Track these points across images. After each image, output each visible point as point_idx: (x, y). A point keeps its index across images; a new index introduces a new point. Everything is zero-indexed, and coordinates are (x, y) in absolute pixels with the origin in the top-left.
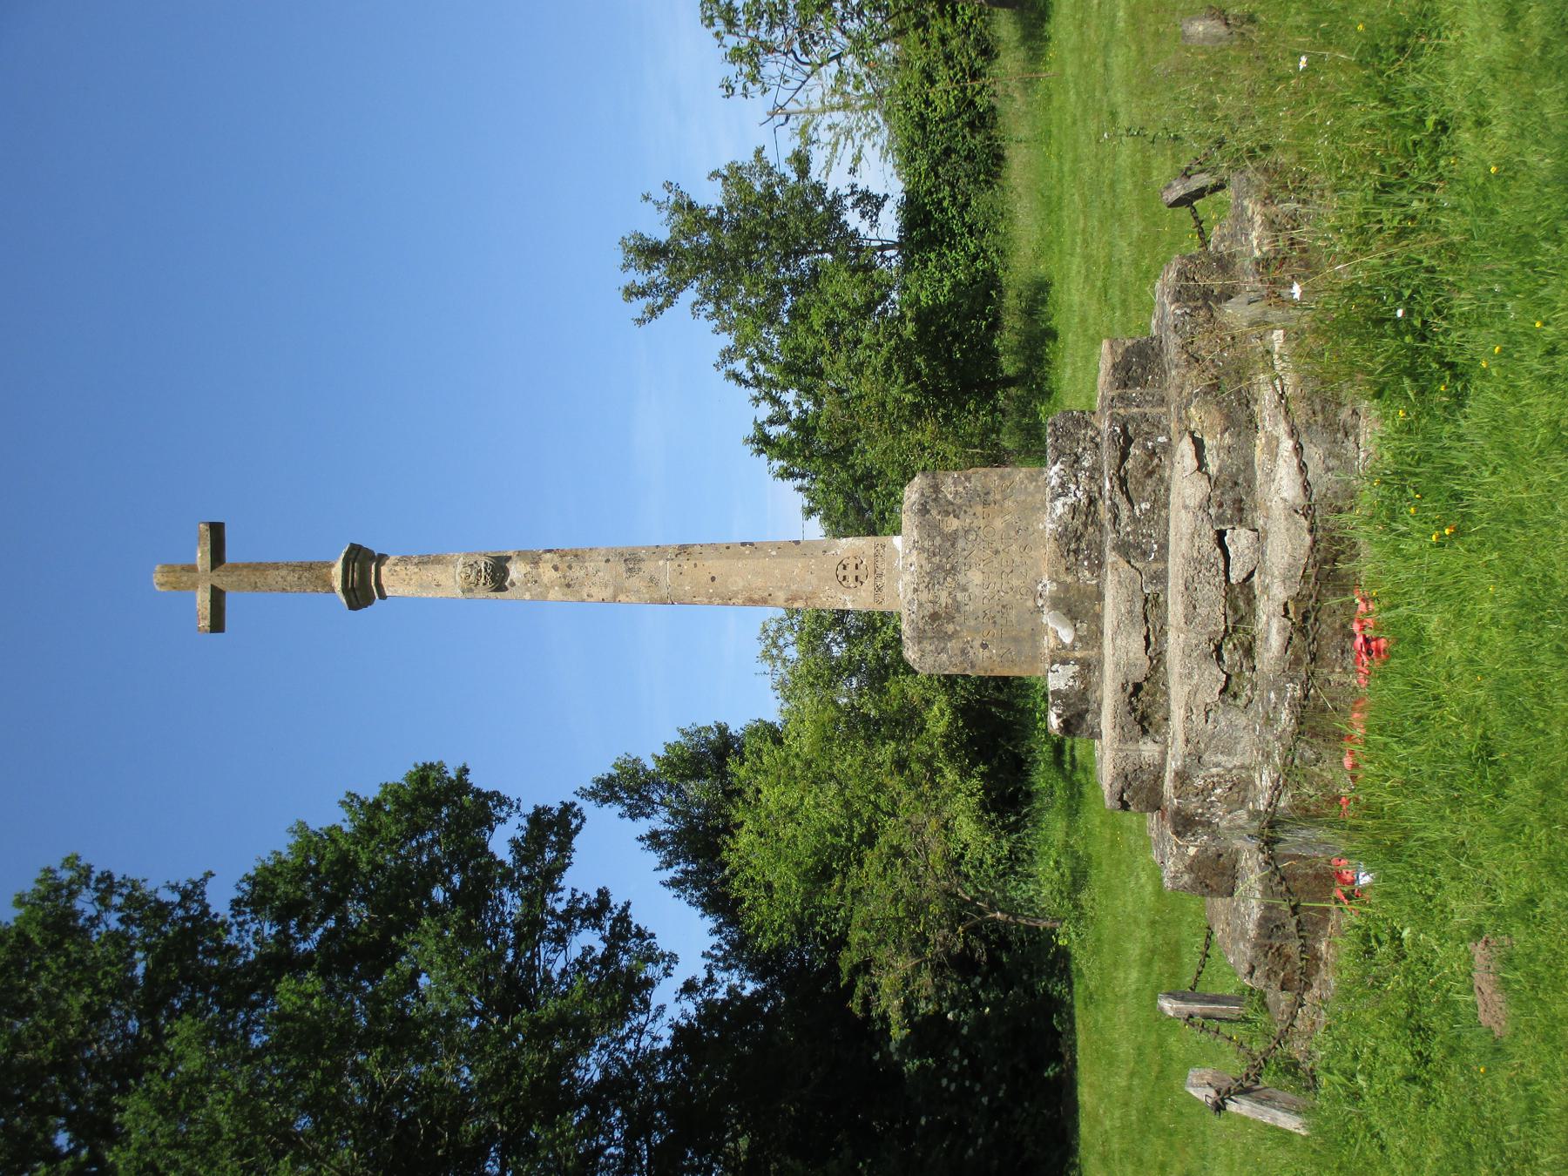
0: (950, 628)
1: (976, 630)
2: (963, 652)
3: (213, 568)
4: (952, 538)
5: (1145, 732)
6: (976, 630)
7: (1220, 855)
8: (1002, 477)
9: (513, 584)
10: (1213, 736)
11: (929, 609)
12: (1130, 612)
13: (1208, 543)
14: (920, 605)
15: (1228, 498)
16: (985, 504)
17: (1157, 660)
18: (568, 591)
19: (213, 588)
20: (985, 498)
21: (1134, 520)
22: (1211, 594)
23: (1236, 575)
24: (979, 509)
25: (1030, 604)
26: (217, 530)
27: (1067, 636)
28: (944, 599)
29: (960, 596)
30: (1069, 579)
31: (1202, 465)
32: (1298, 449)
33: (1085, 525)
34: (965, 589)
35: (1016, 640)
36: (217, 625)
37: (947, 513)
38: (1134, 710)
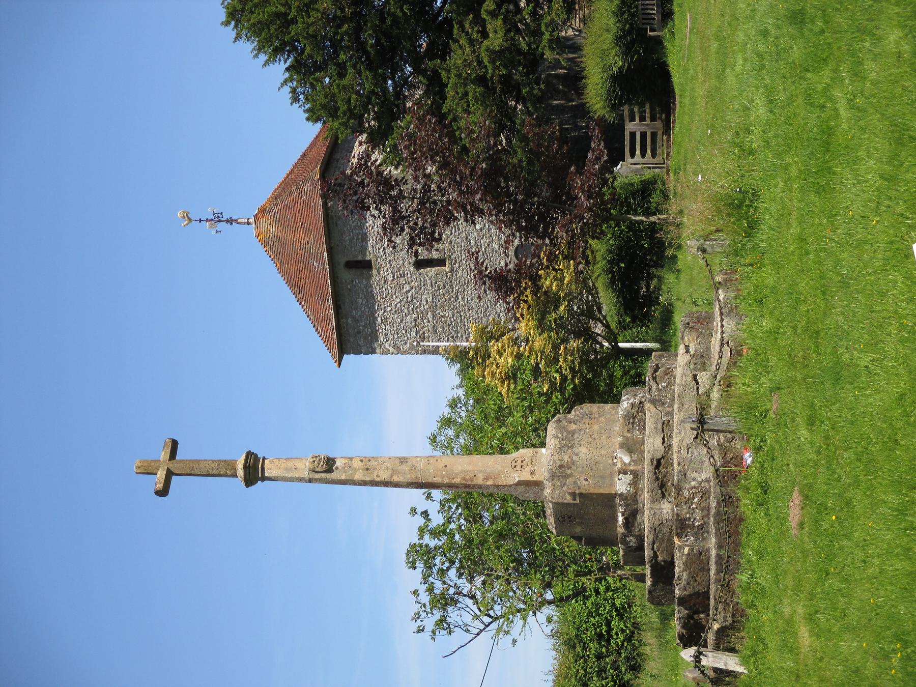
0: (569, 472)
1: (582, 473)
2: (575, 483)
3: (170, 460)
4: (573, 433)
5: (664, 496)
6: (582, 473)
7: (701, 554)
8: (599, 408)
9: (337, 468)
10: (691, 462)
11: (559, 463)
12: (656, 428)
13: (689, 379)
14: (554, 461)
15: (699, 361)
16: (590, 418)
17: (668, 448)
18: (366, 472)
19: (168, 469)
20: (590, 416)
21: (658, 390)
22: (691, 394)
23: (702, 390)
24: (587, 421)
25: (610, 461)
26: (175, 444)
27: (627, 459)
28: (566, 458)
29: (574, 458)
30: (629, 435)
31: (687, 352)
32: (722, 320)
33: (638, 412)
34: (577, 455)
35: (602, 477)
36: (163, 492)
37: (571, 422)
38: (658, 479)
